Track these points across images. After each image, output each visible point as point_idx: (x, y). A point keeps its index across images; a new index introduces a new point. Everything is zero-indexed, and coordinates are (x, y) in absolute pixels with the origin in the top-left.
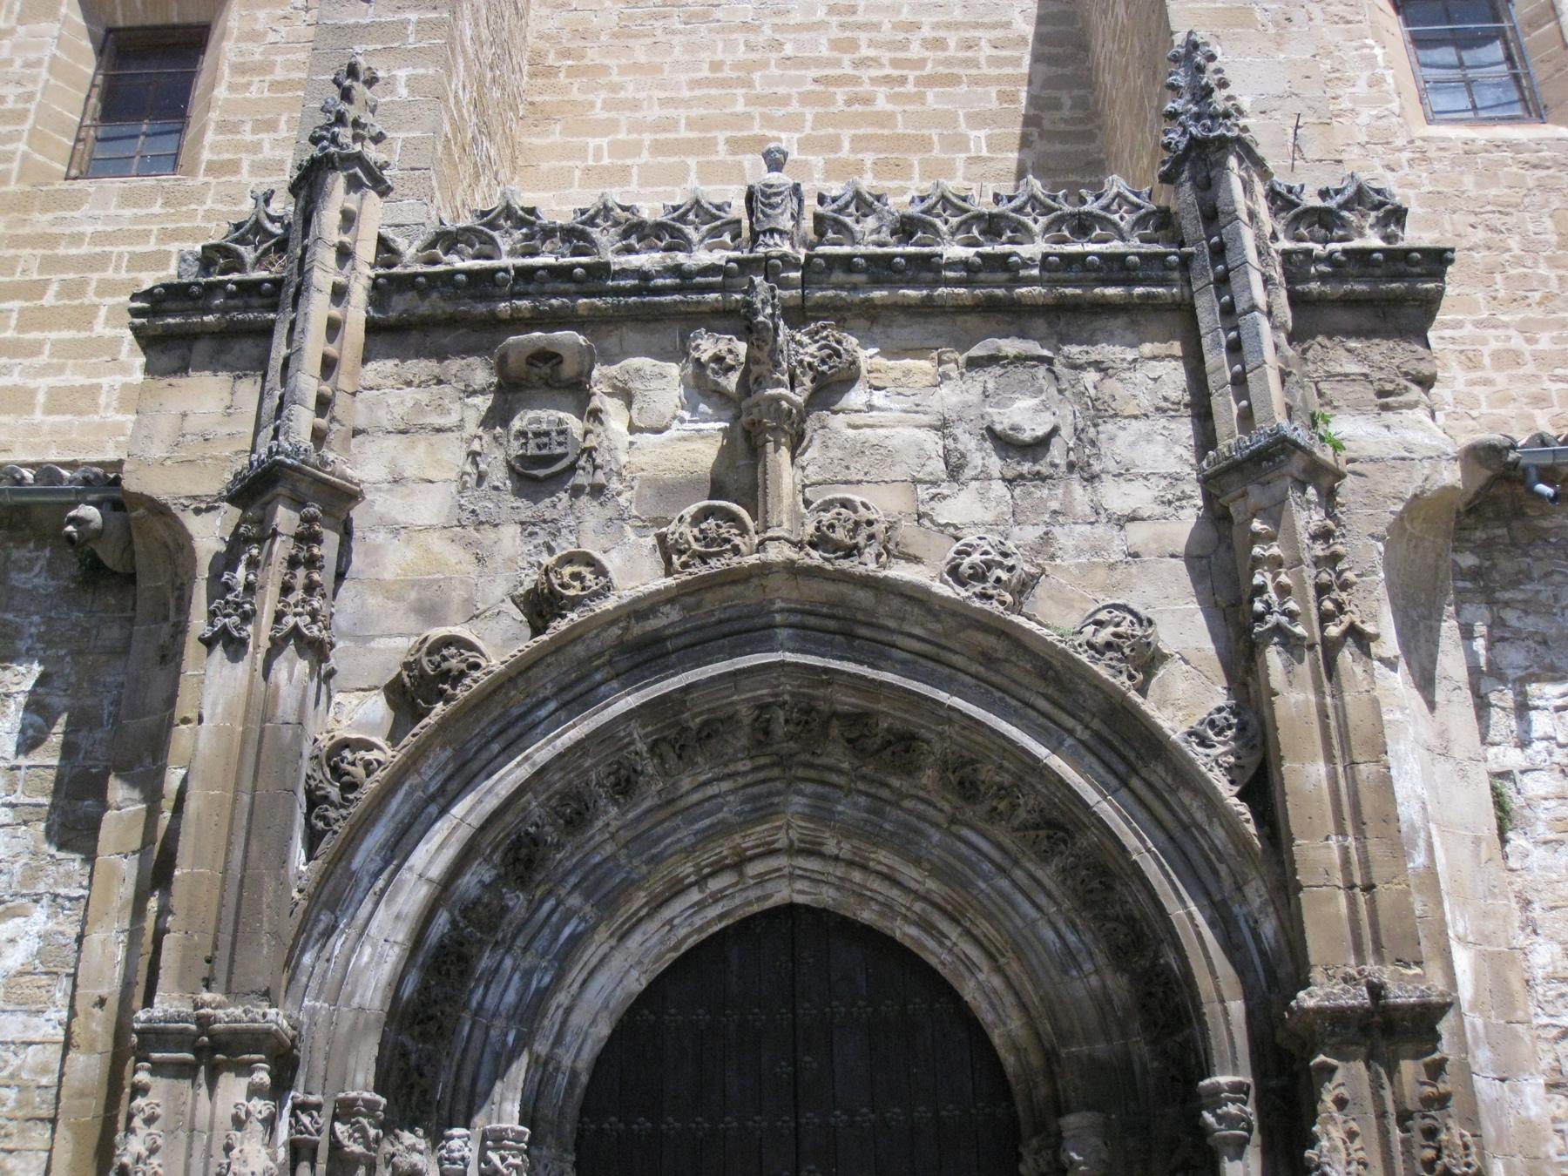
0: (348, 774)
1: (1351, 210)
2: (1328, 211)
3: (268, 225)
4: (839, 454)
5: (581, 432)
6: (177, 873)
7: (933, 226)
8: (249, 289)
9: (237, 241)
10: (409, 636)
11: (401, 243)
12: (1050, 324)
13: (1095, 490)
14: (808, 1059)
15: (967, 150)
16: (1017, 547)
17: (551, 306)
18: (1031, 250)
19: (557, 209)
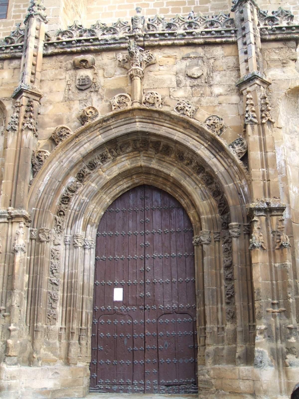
0: (40, 158)
1: (279, 17)
2: (274, 17)
3: (20, 32)
4: (152, 82)
5: (92, 78)
6: (3, 181)
7: (175, 25)
8: (16, 47)
9: (13, 36)
10: (54, 127)
11: (50, 34)
12: (203, 49)
13: (211, 89)
14: (147, 218)
15: (195, 4)
16: (192, 103)
17: (85, 49)
18: (198, 31)
19: (86, 26)
